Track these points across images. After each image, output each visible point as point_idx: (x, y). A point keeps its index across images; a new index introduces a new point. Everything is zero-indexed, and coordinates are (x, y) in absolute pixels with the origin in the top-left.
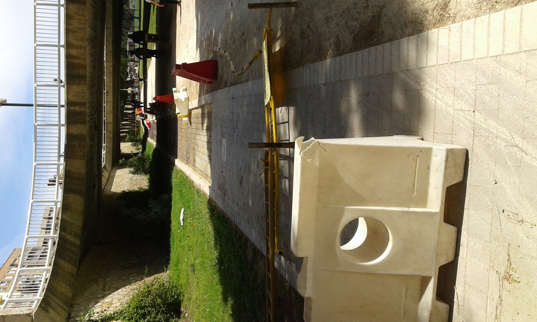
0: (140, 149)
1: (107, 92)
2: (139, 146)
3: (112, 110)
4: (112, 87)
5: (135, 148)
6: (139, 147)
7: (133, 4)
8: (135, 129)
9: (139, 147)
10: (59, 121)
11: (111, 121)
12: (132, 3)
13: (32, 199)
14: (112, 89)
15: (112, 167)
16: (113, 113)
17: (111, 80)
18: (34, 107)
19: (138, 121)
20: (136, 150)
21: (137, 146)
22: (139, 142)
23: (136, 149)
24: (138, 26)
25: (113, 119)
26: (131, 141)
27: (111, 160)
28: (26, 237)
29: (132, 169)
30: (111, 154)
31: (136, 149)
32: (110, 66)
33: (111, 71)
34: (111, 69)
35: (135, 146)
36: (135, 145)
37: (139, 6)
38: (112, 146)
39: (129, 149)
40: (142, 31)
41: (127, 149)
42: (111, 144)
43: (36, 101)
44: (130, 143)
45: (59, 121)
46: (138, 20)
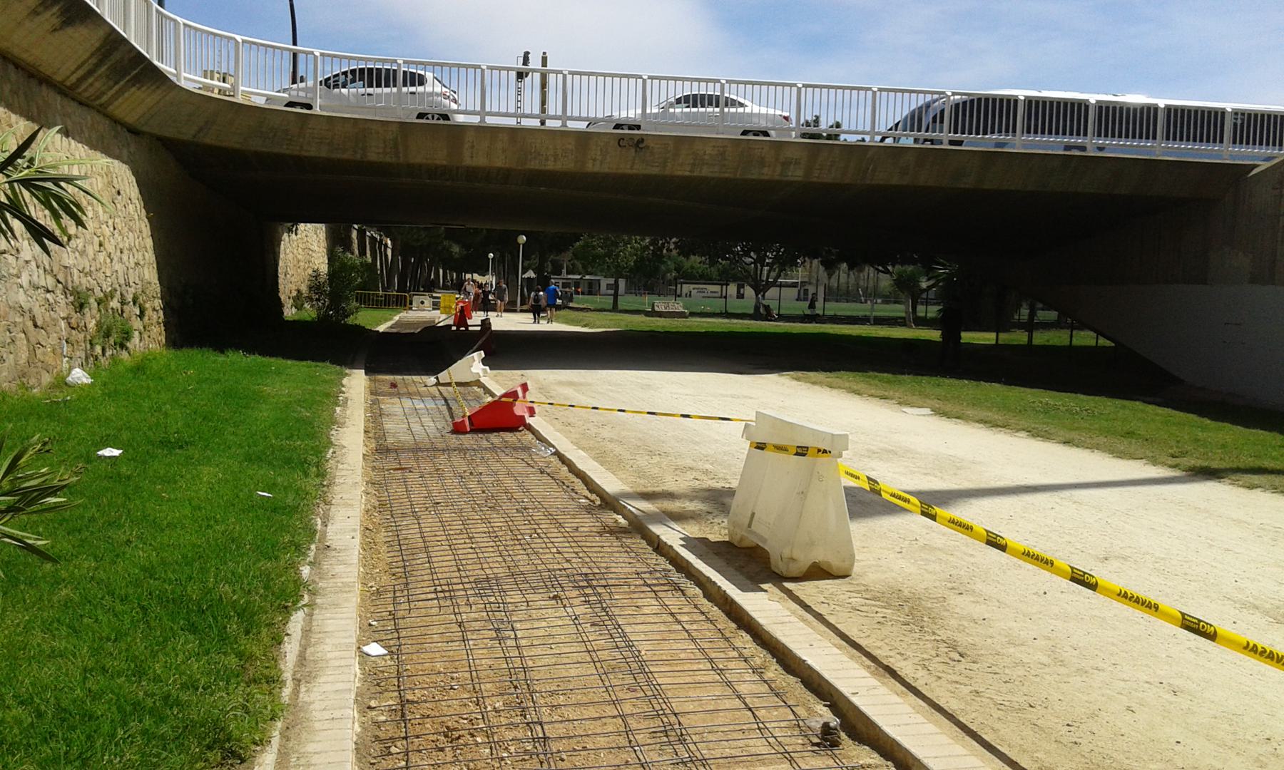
0: (299, 307)
1: (642, 140)
2: (312, 306)
3: (534, 165)
4: (667, 172)
5: (304, 289)
6: (307, 306)
7: (694, 292)
8: (381, 293)
9: (307, 306)
10: (491, 114)
11: (467, 154)
12: (696, 291)
13: (322, 54)
14: (655, 171)
15: (167, 144)
16: (505, 175)
17: (705, 172)
18: (540, 68)
19: (411, 303)
20: (294, 294)
21: (310, 299)
22: (329, 308)
23: (299, 291)
24: (730, 311)
25: (473, 173)
26: (332, 274)
27: (209, 140)
28: (239, 38)
29: (323, 278)
30: (256, 145)
31: (299, 291)
32: (786, 164)
33: (754, 174)
34: (767, 173)
35: (310, 288)
36: (315, 287)
37: (739, 311)
38: (312, 151)
39: (302, 264)
40: (960, 338)
41: (300, 257)
42: (324, 153)
43: (553, 72)
44: (324, 268)
45: (491, 114)
46: (751, 311)
